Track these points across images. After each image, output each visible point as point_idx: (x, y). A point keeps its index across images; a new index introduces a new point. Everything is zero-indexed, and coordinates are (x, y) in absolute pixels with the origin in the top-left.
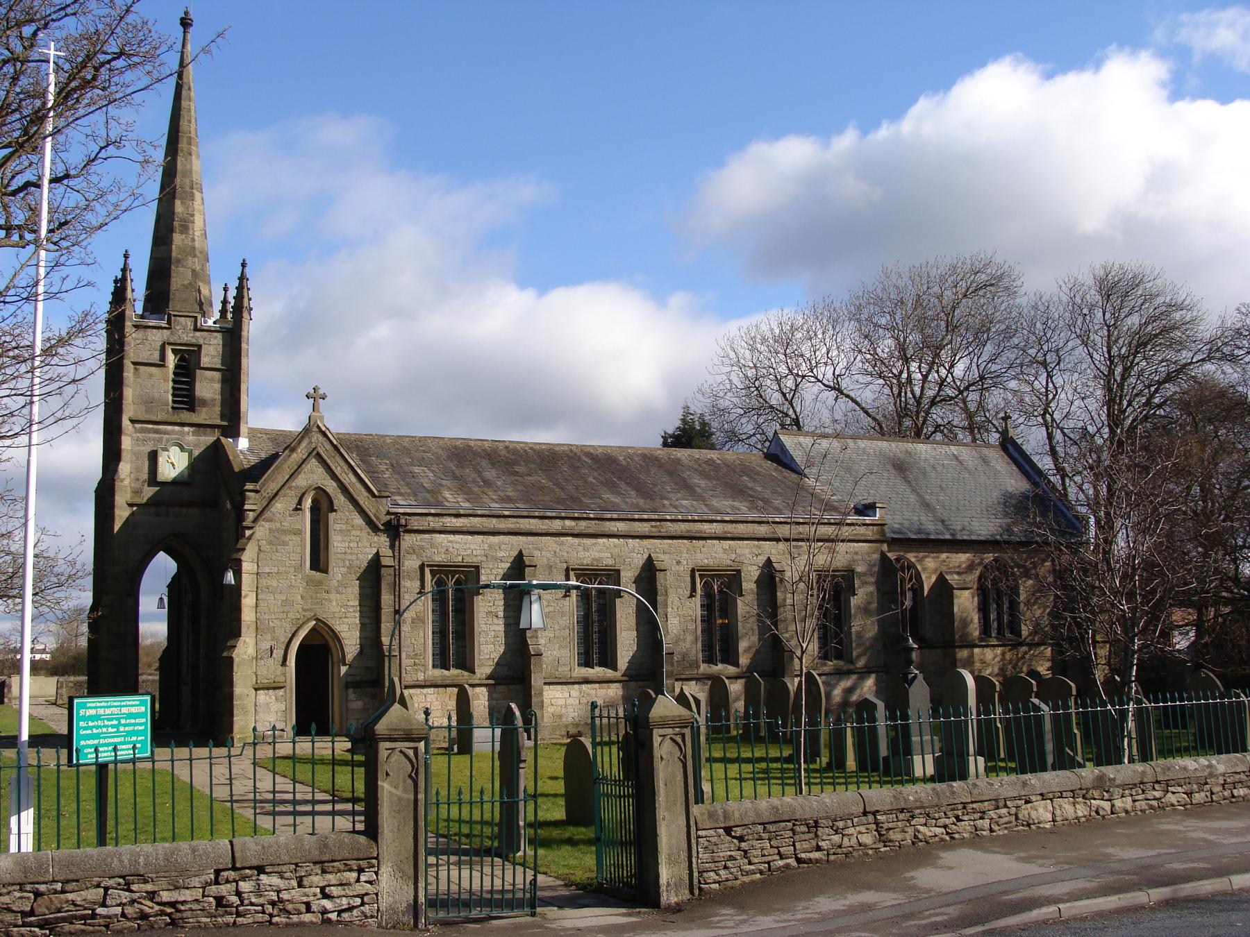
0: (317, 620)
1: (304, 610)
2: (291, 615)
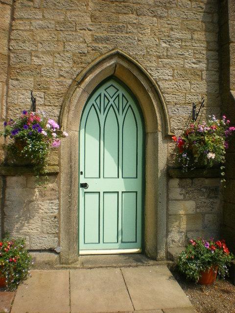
0: (119, 55)
1: (96, 40)
2: (72, 47)
